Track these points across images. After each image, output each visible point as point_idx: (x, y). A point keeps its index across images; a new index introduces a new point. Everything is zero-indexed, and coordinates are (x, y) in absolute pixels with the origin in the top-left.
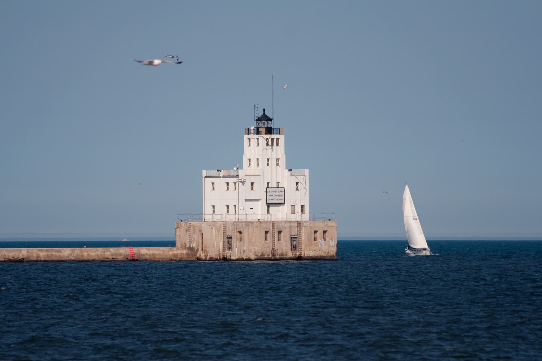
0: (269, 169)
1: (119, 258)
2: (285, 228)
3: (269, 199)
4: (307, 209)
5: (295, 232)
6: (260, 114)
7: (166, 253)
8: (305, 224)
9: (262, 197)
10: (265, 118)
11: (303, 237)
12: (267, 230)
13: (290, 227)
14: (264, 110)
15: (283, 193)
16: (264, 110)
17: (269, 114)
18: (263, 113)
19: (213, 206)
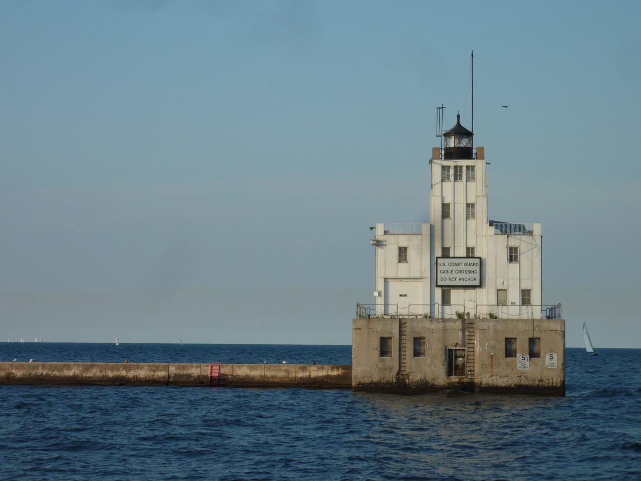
0: (471, 222)
1: (319, 377)
2: (431, 331)
3: (443, 279)
4: (536, 298)
5: (455, 338)
6: (450, 125)
7: (292, 375)
8: (484, 325)
9: (428, 274)
10: (460, 132)
11: (478, 349)
12: (386, 335)
13: (445, 330)
14: (458, 116)
15: (477, 268)
16: (458, 116)
17: (466, 124)
18: (454, 123)
19: (401, 295)
